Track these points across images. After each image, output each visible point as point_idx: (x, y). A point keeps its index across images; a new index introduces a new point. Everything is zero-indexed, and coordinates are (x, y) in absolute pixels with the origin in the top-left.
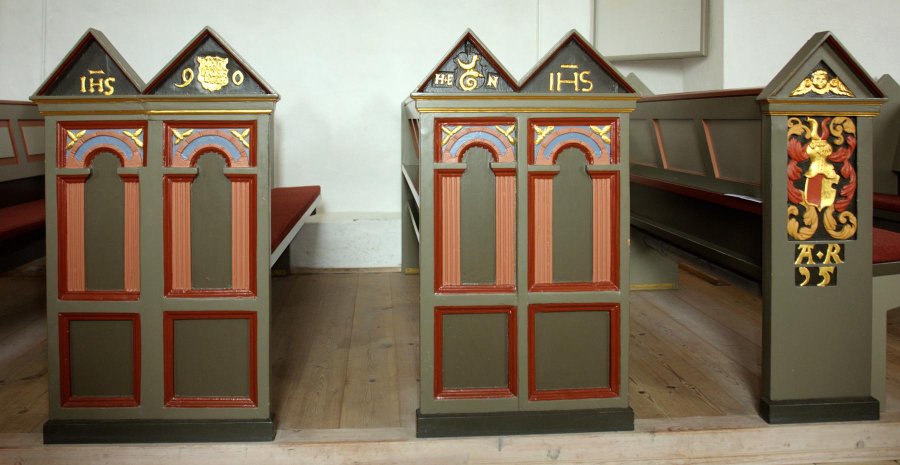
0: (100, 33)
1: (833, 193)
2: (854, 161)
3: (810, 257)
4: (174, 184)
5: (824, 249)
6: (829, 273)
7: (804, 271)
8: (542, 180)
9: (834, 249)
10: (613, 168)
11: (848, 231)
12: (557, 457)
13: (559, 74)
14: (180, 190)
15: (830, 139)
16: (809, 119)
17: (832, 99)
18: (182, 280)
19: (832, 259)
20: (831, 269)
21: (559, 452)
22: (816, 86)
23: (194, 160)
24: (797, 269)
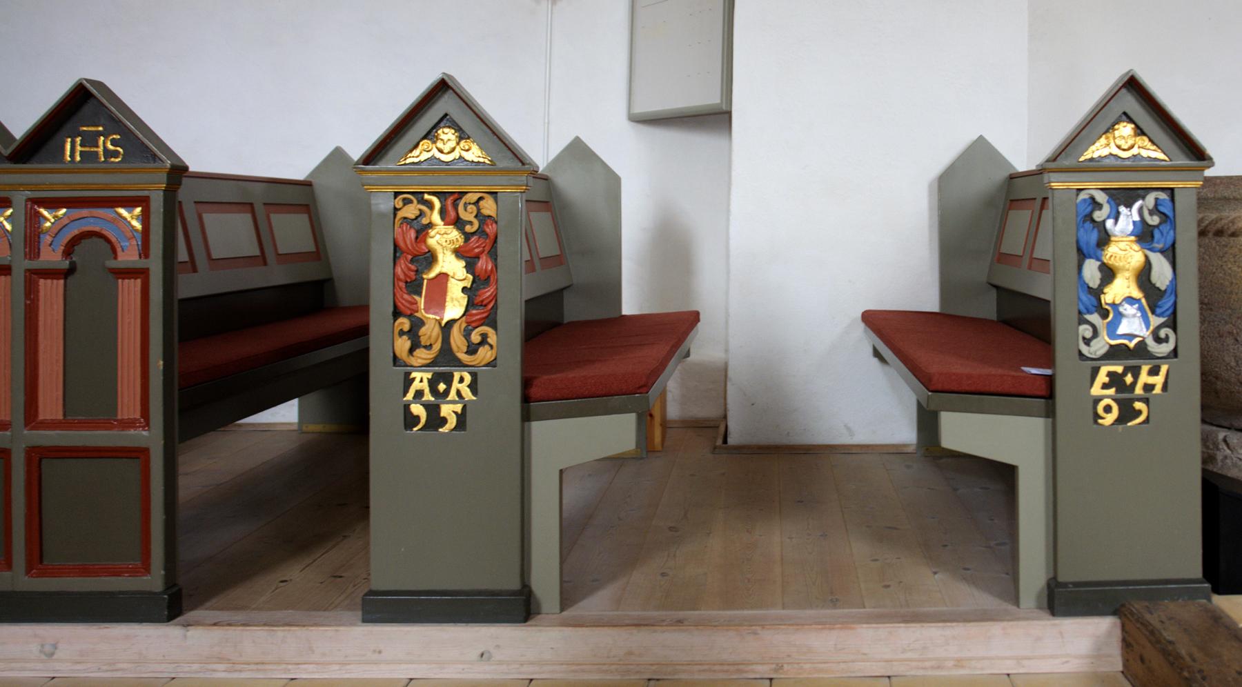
0: (100, 85)
1: (464, 300)
2: (493, 254)
3: (427, 391)
4: (42, 281)
5: (448, 379)
6: (455, 413)
7: (417, 409)
8: (49, 281)
9: (462, 380)
10: (142, 263)
11: (1165, 349)
12: (52, 654)
13: (78, 140)
14: (51, 291)
15: (458, 223)
16: (426, 196)
17: (1137, 166)
18: (50, 405)
19: (459, 393)
20: (459, 408)
21: (55, 646)
22: (441, 151)
23: (68, 251)
24: (407, 407)
